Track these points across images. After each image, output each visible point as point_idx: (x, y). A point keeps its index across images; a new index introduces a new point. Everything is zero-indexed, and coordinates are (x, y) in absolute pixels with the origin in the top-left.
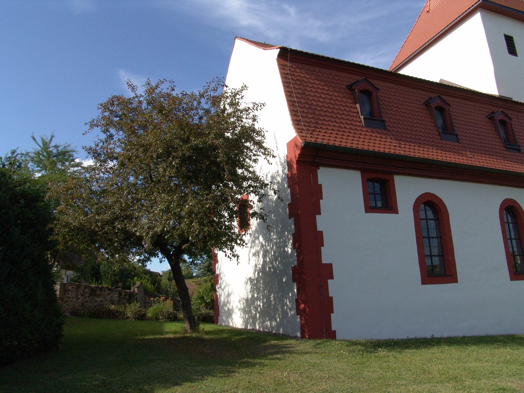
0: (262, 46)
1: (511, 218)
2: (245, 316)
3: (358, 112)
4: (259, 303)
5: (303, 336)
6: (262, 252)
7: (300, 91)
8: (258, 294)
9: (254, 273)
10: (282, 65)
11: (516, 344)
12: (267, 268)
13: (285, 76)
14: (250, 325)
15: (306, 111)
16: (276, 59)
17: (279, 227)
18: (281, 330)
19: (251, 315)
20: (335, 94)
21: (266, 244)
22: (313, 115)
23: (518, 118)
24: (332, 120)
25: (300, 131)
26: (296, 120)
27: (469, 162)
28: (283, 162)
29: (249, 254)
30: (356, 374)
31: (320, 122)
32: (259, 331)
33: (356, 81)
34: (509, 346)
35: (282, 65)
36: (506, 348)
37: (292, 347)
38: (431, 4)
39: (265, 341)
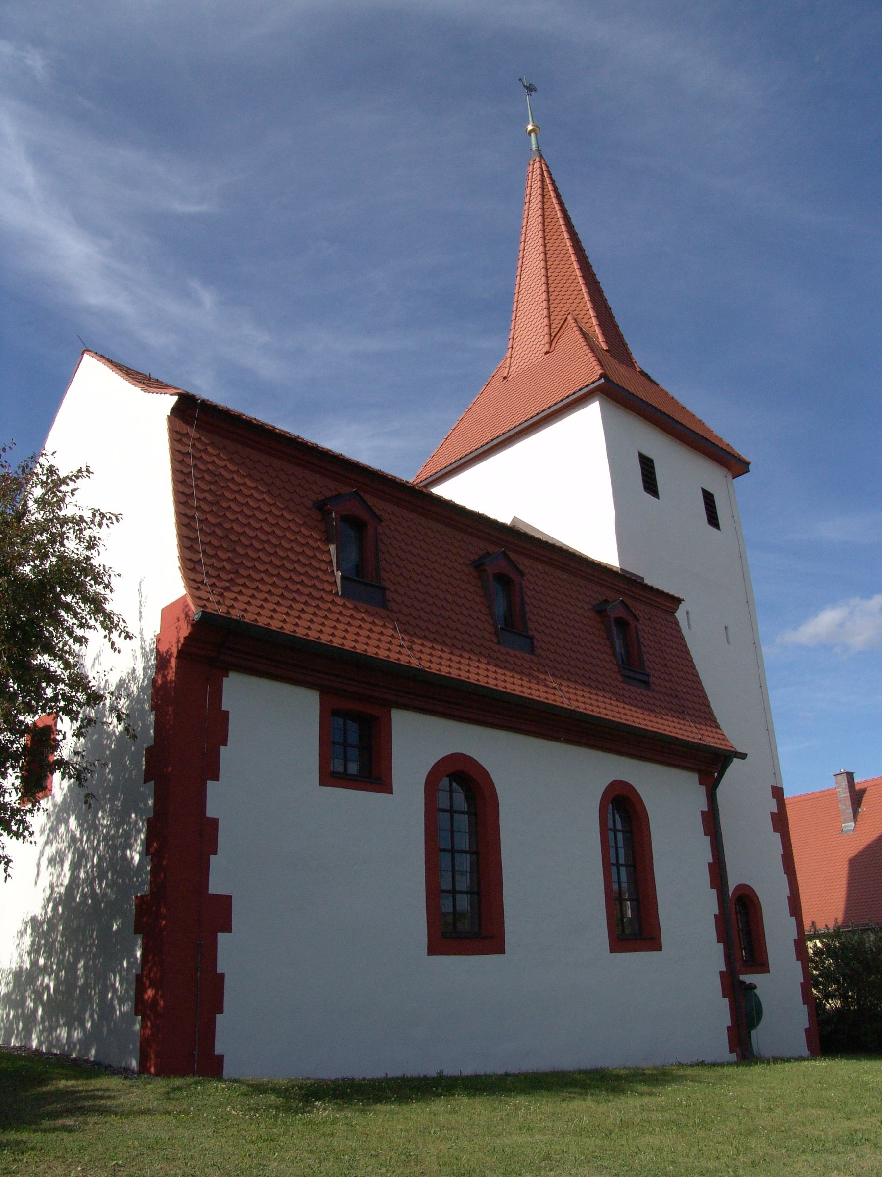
0: (140, 382)
1: (621, 819)
2: (8, 1015)
3: (331, 561)
4: (46, 980)
5: (143, 1068)
6: (70, 856)
7: (209, 497)
8: (48, 958)
9: (45, 908)
10: (177, 432)
11: (606, 1090)
12: (79, 896)
13: (181, 457)
14: (16, 1038)
15: (216, 543)
16: (166, 417)
17: (119, 799)
18: (93, 1052)
19: (23, 1011)
20: (286, 515)
21: (82, 837)
22: (230, 554)
23: (650, 619)
24: (271, 569)
25: (196, 585)
26: (190, 560)
27: (549, 696)
28: (148, 649)
29: (39, 859)
30: (250, 1167)
31: (242, 572)
32: (37, 1051)
33: (336, 493)
34: (592, 1095)
35: (177, 432)
36: (584, 1100)
37: (109, 1097)
38: (513, 365)
39: (42, 1080)
